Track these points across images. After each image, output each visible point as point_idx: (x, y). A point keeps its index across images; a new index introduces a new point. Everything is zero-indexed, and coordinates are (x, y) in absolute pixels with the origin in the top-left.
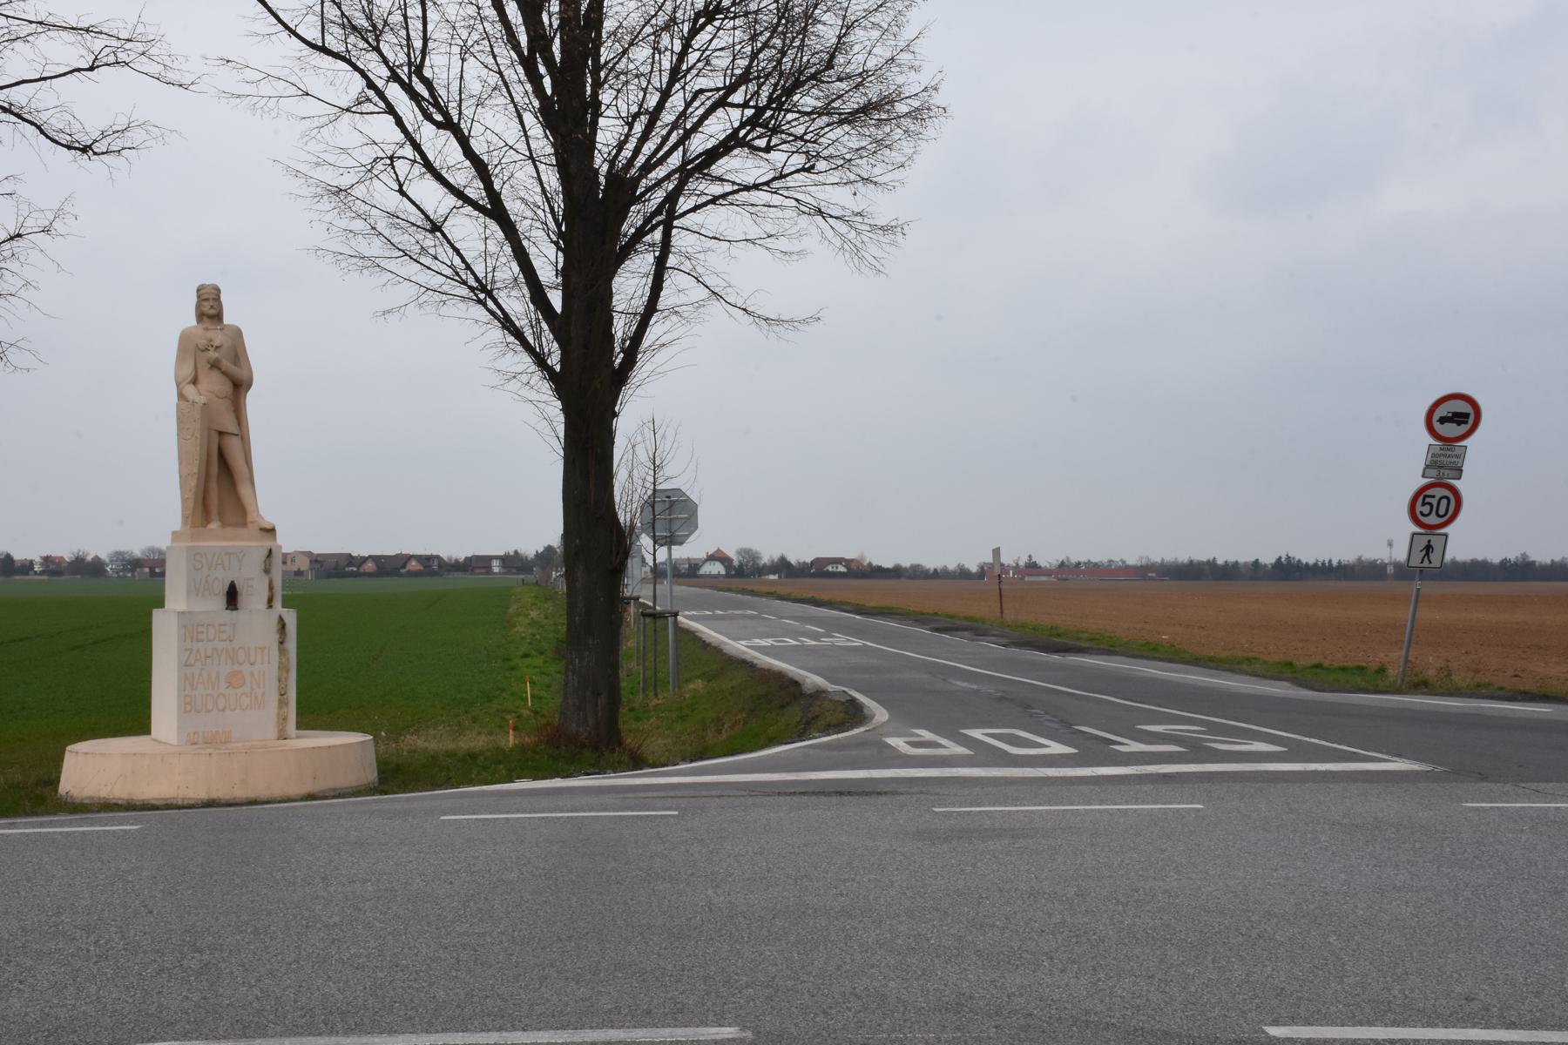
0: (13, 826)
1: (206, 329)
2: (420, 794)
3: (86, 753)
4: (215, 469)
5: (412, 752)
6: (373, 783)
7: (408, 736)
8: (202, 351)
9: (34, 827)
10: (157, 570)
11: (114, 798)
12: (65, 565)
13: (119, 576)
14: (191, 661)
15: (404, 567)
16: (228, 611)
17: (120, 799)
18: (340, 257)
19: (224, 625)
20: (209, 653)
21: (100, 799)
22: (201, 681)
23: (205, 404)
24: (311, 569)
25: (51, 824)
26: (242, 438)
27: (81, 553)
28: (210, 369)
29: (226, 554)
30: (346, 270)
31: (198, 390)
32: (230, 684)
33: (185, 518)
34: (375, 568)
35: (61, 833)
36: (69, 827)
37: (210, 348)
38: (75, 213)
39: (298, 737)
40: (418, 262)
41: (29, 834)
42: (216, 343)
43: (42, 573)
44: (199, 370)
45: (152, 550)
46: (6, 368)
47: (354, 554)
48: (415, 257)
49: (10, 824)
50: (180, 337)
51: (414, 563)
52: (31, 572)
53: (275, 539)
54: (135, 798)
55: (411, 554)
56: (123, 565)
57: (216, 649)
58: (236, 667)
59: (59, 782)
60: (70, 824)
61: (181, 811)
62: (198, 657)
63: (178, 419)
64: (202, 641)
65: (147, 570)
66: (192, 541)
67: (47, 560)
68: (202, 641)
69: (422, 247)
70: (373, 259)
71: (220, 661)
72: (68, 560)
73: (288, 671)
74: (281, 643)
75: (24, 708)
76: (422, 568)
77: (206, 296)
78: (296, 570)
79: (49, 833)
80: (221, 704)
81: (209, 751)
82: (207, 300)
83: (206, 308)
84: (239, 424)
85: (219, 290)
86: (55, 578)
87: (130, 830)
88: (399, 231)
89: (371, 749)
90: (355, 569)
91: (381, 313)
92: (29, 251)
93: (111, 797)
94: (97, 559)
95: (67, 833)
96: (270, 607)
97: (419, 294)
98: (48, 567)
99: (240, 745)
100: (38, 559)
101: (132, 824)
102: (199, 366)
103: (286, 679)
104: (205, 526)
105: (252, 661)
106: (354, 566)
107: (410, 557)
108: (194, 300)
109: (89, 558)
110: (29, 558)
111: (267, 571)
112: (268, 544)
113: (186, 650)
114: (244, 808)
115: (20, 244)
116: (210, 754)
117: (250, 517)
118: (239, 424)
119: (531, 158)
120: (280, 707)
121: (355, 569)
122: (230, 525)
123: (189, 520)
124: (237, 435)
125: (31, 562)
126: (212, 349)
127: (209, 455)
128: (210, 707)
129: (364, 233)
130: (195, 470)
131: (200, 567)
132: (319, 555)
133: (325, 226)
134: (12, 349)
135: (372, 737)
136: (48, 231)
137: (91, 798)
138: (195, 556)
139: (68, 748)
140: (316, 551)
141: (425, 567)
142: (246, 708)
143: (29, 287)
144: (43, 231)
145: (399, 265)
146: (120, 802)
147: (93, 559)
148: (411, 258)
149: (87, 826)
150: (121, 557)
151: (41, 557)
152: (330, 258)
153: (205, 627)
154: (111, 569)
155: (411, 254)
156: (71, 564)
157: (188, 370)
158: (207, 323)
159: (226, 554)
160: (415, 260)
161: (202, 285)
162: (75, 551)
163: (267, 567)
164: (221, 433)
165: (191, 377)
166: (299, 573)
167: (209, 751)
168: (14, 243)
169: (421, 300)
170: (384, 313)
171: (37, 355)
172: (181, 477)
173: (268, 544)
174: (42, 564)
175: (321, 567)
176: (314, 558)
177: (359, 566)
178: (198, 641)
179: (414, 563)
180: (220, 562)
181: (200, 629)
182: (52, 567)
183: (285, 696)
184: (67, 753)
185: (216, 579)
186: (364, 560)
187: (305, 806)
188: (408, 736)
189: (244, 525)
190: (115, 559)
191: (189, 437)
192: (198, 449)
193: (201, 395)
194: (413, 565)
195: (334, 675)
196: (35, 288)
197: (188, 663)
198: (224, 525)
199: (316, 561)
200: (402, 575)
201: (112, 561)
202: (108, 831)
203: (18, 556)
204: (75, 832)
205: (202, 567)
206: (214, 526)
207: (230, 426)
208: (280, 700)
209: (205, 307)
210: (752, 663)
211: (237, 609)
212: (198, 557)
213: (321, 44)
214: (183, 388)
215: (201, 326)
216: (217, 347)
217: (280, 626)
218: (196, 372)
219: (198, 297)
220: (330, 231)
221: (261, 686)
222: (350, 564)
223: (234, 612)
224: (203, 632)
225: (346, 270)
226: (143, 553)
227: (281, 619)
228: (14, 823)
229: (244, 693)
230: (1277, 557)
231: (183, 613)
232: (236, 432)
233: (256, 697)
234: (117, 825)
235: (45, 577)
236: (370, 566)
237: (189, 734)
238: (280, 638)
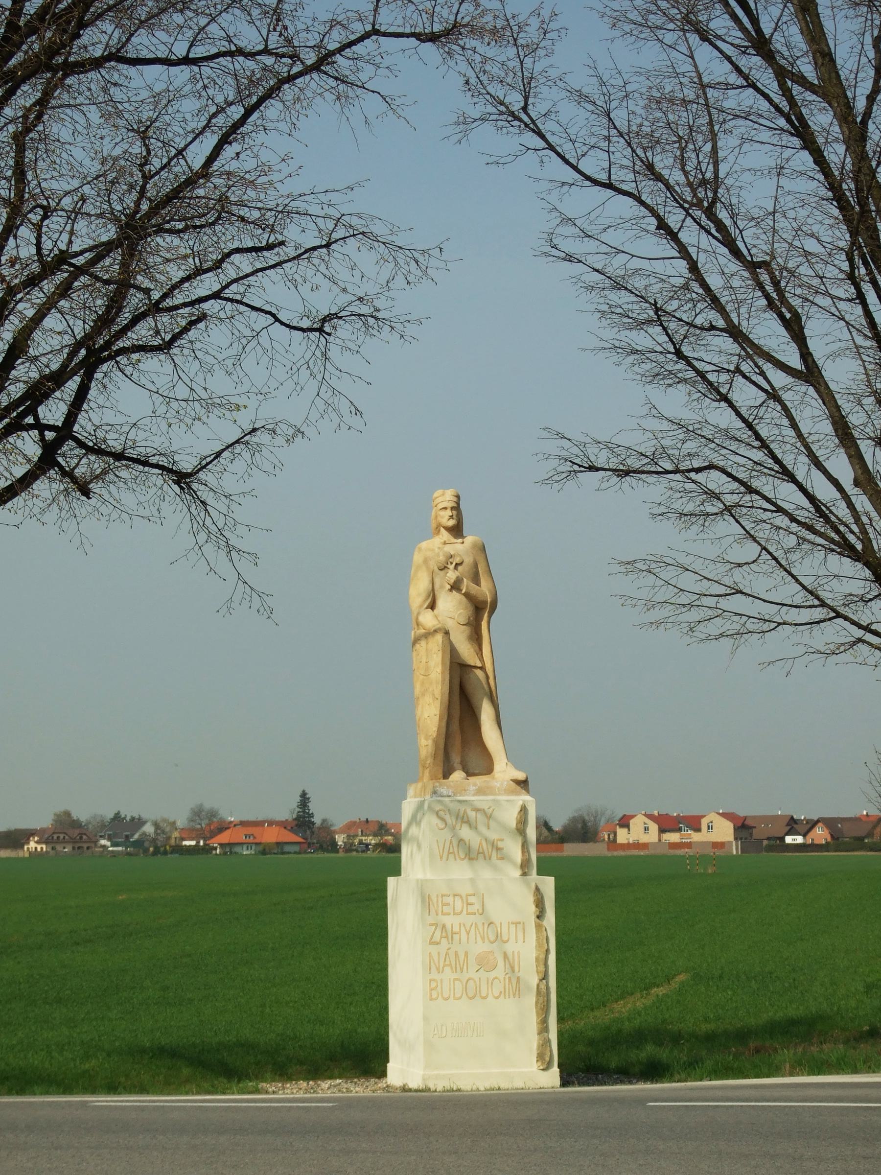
22: (447, 962)
96: (524, 874)
106: (798, 834)
113: (431, 925)
119: (328, 245)
153: (451, 896)
178: (443, 914)
206: (458, 776)
213: (676, 231)
224: (448, 904)
227: (537, 889)
230: (300, 792)
236: (820, 834)
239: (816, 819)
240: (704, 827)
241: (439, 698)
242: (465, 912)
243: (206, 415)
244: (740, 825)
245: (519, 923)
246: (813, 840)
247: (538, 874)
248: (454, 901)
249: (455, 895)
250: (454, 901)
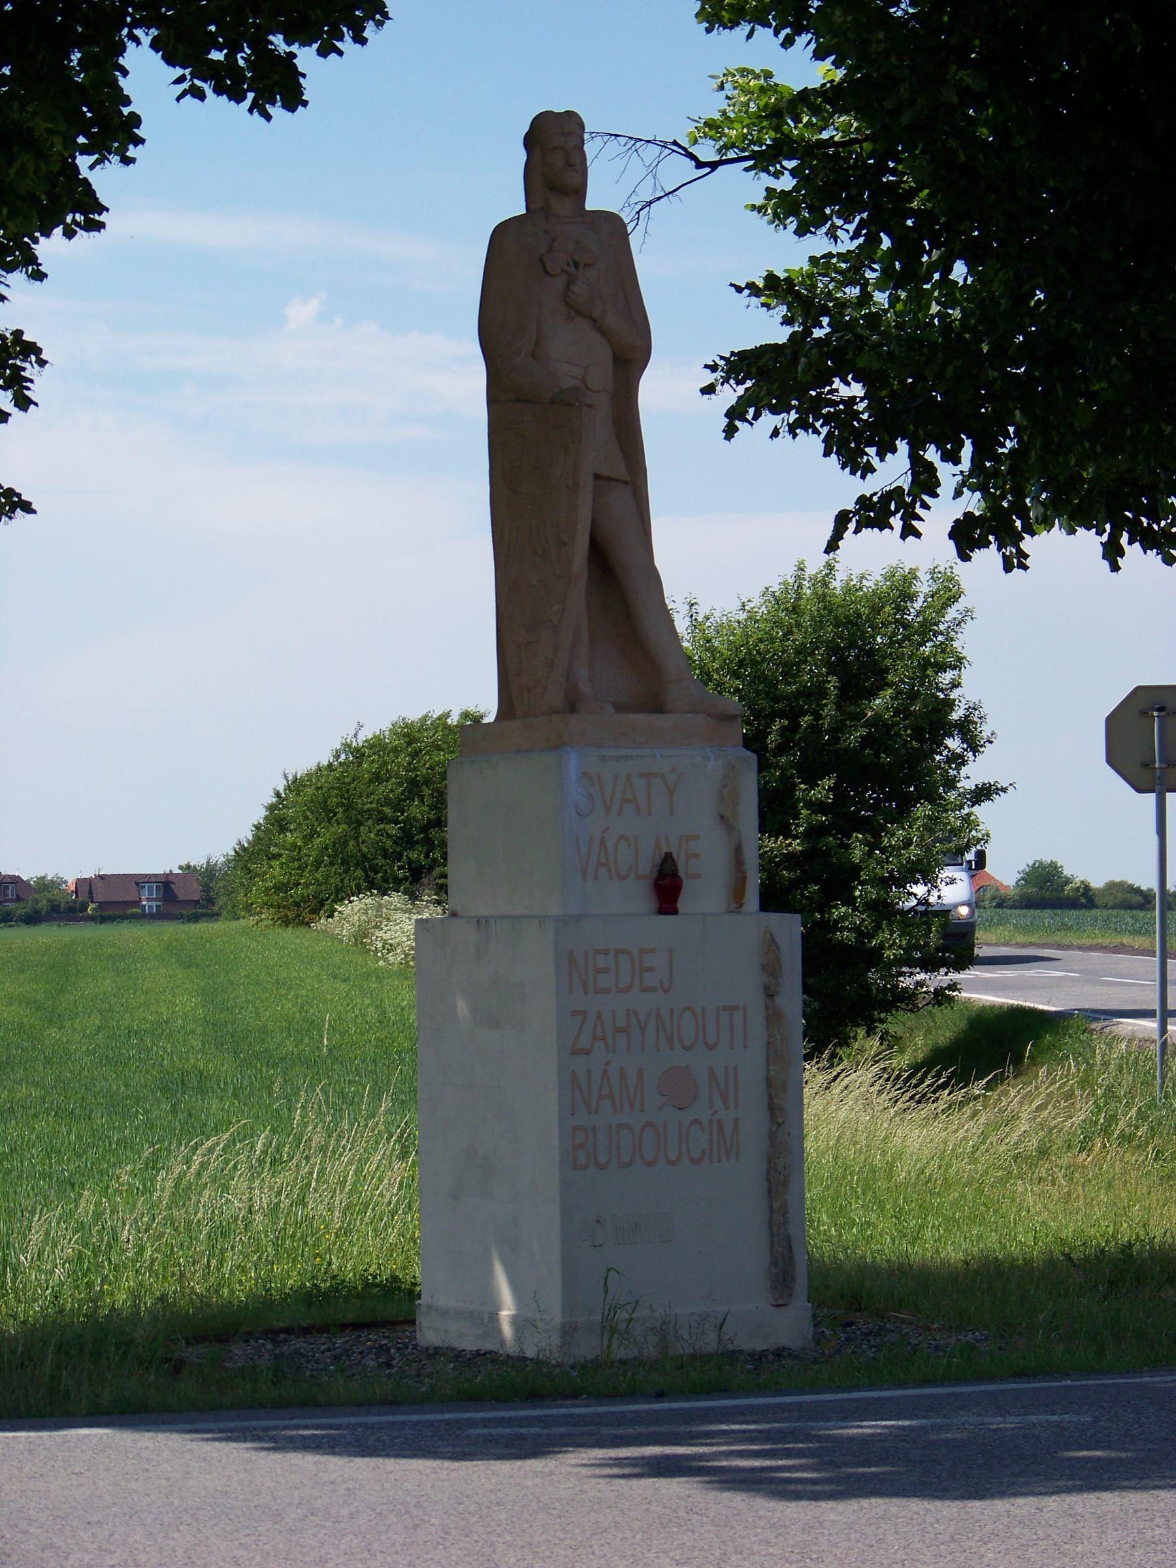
14: (584, 1043)
19: (653, 951)
57: (636, 1013)
62: (599, 1033)
64: (606, 991)
68: (606, 991)
128: (602, 1159)
142: (701, 1159)
159: (642, 775)
180: (629, 795)
181: (602, 962)
210: (350, 1456)
221: (732, 1105)
224: (605, 971)
242: (636, 987)
248: (617, 965)
249: (618, 952)
250: (617, 965)
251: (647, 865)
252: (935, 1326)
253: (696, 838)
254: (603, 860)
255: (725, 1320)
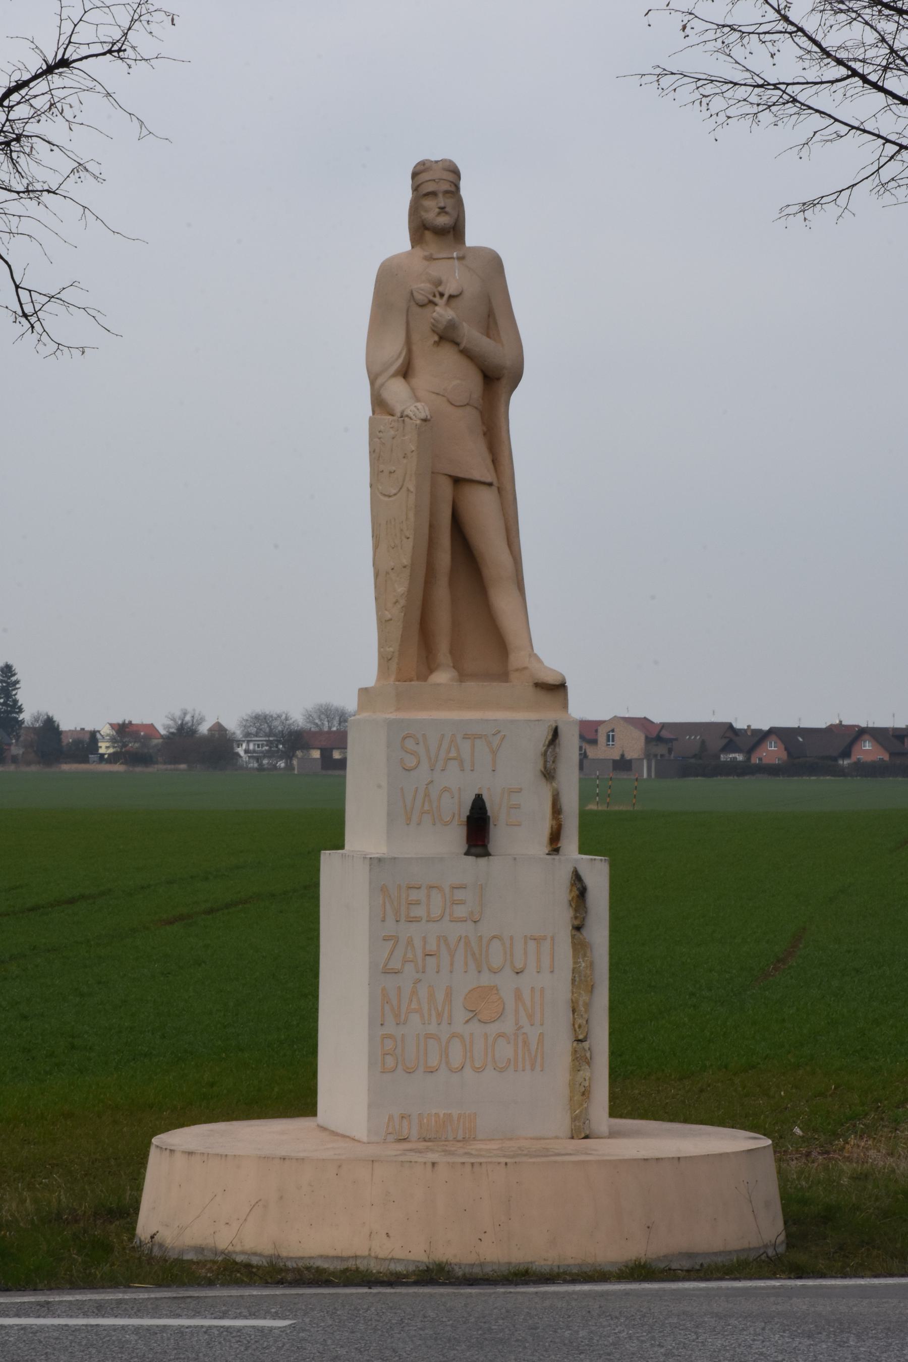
0: (46, 1309)
1: (430, 258)
2: (876, 1281)
3: (190, 1153)
4: (444, 558)
5: (861, 1178)
6: (775, 1246)
7: (852, 1140)
8: (422, 306)
9: (86, 1315)
10: (337, 755)
11: (243, 1253)
12: (155, 742)
13: (261, 768)
14: (395, 964)
15: (846, 753)
16: (471, 859)
17: (255, 1254)
18: (709, 89)
19: (462, 887)
20: (432, 946)
21: (216, 1252)
22: (414, 1006)
23: (425, 420)
24: (648, 756)
25: (118, 1308)
26: (499, 490)
27: (188, 718)
28: (437, 344)
29: (466, 737)
30: (722, 117)
31: (413, 390)
32: (474, 1015)
33: (384, 660)
34: (784, 755)
35: (137, 1330)
36: (153, 1317)
37: (437, 299)
38: (171, 10)
39: (613, 1134)
40: (881, 89)
41: (77, 1329)
42: (450, 288)
43: (113, 758)
44: (415, 348)
45: (326, 712)
46: (40, 347)
47: (739, 725)
48: (873, 78)
49: (40, 1305)
50: (381, 266)
51: (867, 746)
52: (92, 757)
53: (565, 706)
54: (284, 1254)
55: (863, 725)
56: (269, 743)
58: (486, 979)
59: (137, 1210)
60: (155, 1312)
61: (374, 1290)
63: (372, 452)
64: (417, 920)
65: (316, 754)
66: (398, 709)
67: (123, 730)
68: (417, 920)
69: (892, 51)
70: (783, 87)
71: (452, 964)
72: (163, 732)
73: (591, 989)
74: (578, 928)
75: (73, 1047)
76: (886, 757)
77: (430, 187)
78: (617, 757)
79: (115, 1328)
80: (456, 1058)
81: (432, 1157)
82: (433, 194)
83: (432, 215)
84: (495, 461)
85: (456, 173)
86: (138, 769)
87: (271, 1329)
88: (842, 17)
89: (769, 1166)
90: (740, 757)
91: (796, 208)
92: (83, 95)
93: (238, 1248)
94: (219, 729)
95: (149, 1329)
97: (882, 162)
98: (125, 745)
99: (494, 1146)
100: (106, 730)
101: (275, 1316)
102: (415, 337)
103: (587, 1006)
104: (424, 678)
105: (519, 965)
106: (738, 751)
107: (861, 733)
108: (406, 195)
109: (204, 729)
110: (89, 727)
111: (549, 774)
112: (551, 716)
113: (386, 939)
114: (501, 1290)
115: (67, 82)
116: (434, 1164)
117: (517, 659)
118: (495, 461)
120: (576, 1069)
121: (740, 757)
122: (474, 676)
123: (394, 666)
124: (490, 484)
125: (93, 735)
126: (441, 302)
127: (432, 527)
128: (433, 1061)
129: (760, 30)
130: (406, 561)
131: (413, 764)
132: (664, 726)
133: (678, 20)
134: (51, 307)
135: (770, 1142)
136: (119, 51)
137: (200, 1250)
138: (404, 738)
139: (155, 1140)
140: (659, 717)
141: (891, 754)
143: (83, 174)
144: (110, 52)
145: (839, 95)
146: (255, 1261)
147: (210, 730)
148: (864, 79)
149: (189, 1317)
150: (265, 727)
151: (112, 725)
152: (687, 92)
154: (246, 751)
155: (866, 70)
156: (170, 739)
157: (393, 348)
158: (433, 246)
160: (875, 85)
161: (423, 163)
162: (178, 713)
163: (549, 765)
164: (457, 481)
165: (400, 361)
166: (623, 764)
167: (432, 1157)
168: (55, 80)
169: (886, 173)
170: (805, 206)
171: (99, 317)
172: (377, 575)
173: (551, 716)
174: (113, 740)
175: (670, 751)
176: (654, 734)
177: (750, 752)
178: (411, 920)
179: (867, 746)
182: (133, 746)
183: (586, 1045)
184: (153, 1152)
185: (446, 789)
186: (761, 737)
187: (627, 1293)
188: (852, 1140)
189: (504, 676)
190: (253, 730)
191: (394, 491)
192: (411, 515)
193: (418, 400)
194: (867, 749)
195: (692, 994)
196: (96, 177)
197: (391, 965)
198: (463, 676)
199: (659, 739)
200: (841, 773)
201: (248, 735)
202: (227, 1329)
203: (67, 723)
204: (165, 1328)
205: (419, 763)
206: (442, 677)
207: (478, 467)
208: (575, 1051)
209: (426, 211)
211: (487, 854)
212: (410, 744)
214: (382, 385)
215: (420, 252)
216: (451, 297)
217: (576, 892)
218: (410, 352)
219: (415, 189)
220: (688, 30)
222: (730, 746)
223: (482, 861)
224: (418, 903)
225: (722, 117)
226: (309, 717)
227: (577, 878)
228: (48, 1303)
229: (500, 1035)
231: (380, 860)
232: (489, 479)
233: (526, 1043)
234: (246, 1318)
235: (118, 768)
236: (772, 752)
237: (391, 1118)
238: (576, 918)
239: (766, 728)
240: (602, 739)
241: (411, 537)
242: (447, 917)
243: (786, 27)
244: (654, 734)
245: (544, 938)
246: (760, 759)
247: (582, 851)
251: (426, 263)
252: (625, 1027)
253: (519, 791)
254: (410, 955)
255: (434, 393)
